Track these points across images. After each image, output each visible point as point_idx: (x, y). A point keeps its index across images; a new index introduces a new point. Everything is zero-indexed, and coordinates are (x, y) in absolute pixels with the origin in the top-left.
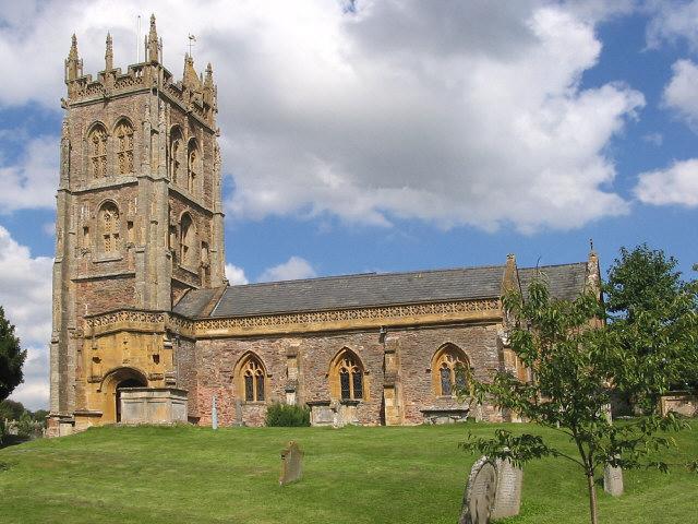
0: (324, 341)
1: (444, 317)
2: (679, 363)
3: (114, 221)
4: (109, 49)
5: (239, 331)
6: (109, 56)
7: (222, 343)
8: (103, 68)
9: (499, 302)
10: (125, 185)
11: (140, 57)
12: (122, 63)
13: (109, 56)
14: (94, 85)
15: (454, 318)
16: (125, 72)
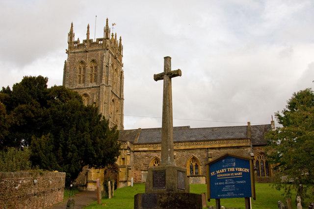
0: (185, 153)
1: (229, 145)
2: (6, 115)
3: (113, 106)
4: (88, 31)
5: (152, 149)
6: (88, 34)
7: (145, 154)
8: (85, 39)
9: (249, 140)
10: (93, 87)
11: (102, 35)
12: (94, 37)
13: (88, 34)
14: (81, 45)
15: (233, 146)
16: (95, 41)
